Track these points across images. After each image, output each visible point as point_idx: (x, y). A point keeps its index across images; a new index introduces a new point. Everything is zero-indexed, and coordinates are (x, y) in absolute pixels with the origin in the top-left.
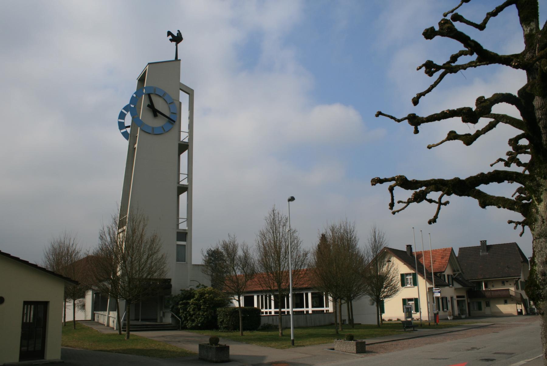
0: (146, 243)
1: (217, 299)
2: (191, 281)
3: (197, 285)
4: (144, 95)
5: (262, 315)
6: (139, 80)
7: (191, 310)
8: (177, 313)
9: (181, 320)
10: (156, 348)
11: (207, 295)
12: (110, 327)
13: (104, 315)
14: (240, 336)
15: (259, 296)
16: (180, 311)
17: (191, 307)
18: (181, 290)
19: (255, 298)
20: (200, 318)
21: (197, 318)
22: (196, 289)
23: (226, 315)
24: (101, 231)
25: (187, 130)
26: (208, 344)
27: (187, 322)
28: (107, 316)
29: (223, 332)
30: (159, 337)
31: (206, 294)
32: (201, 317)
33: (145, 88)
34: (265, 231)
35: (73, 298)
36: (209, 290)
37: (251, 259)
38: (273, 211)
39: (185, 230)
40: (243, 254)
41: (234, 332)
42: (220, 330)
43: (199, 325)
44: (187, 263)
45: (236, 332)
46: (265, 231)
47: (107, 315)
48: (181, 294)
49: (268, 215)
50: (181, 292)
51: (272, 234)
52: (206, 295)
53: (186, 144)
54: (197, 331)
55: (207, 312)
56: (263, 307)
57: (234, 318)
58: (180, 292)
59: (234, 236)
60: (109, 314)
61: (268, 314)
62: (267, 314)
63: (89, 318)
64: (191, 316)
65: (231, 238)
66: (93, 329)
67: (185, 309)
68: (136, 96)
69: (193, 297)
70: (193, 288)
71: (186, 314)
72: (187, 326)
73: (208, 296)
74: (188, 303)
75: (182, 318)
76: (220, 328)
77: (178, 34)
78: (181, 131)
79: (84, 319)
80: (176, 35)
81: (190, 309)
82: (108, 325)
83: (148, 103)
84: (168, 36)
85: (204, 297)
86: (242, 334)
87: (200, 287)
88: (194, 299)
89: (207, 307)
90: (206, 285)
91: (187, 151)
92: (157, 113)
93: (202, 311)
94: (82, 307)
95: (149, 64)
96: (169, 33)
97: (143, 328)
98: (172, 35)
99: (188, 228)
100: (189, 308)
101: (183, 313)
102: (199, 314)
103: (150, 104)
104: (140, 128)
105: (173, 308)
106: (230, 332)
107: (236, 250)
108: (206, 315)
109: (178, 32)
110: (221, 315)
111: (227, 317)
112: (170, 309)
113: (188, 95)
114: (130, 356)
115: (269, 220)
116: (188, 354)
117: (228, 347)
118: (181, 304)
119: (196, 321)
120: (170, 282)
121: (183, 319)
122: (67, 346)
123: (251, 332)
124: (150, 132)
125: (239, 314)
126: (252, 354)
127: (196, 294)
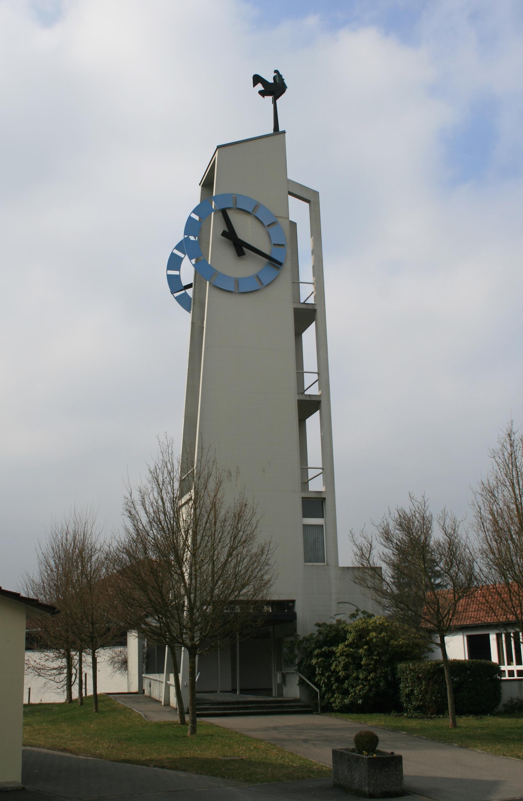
0: (225, 520)
1: (396, 643)
2: (338, 603)
3: (352, 612)
4: (213, 213)
5: (503, 678)
6: (203, 186)
7: (340, 668)
8: (311, 675)
9: (321, 690)
10: (244, 758)
11: (374, 634)
12: (171, 707)
13: (160, 681)
14: (450, 727)
15: (501, 634)
16: (316, 670)
17: (339, 662)
18: (318, 625)
19: (493, 638)
20: (361, 686)
21: (353, 687)
22: (349, 621)
23: (419, 678)
25: (311, 279)
26: (353, 751)
27: (333, 696)
28: (164, 685)
29: (412, 717)
30: (267, 729)
31: (370, 631)
32: (363, 685)
33: (216, 199)
34: (493, 483)
35: (91, 646)
36: (378, 622)
37: (464, 550)
38: (509, 435)
39: (320, 492)
40: (445, 537)
41: (439, 717)
42: (405, 715)
43: (360, 702)
44: (327, 565)
45: (443, 717)
46: (493, 483)
47: (164, 681)
48: (317, 633)
49: (499, 446)
50: (317, 628)
51: (510, 488)
52: (371, 634)
53: (310, 307)
54: (355, 716)
55: (376, 672)
56: (512, 661)
57: (437, 687)
58: (315, 630)
59: (423, 497)
61: (516, 677)
62: (514, 676)
63: (135, 688)
65: (416, 503)
66: (132, 710)
67: (326, 667)
68: (200, 218)
69: (345, 639)
70: (343, 619)
71: (329, 678)
72: (333, 705)
73: (376, 637)
74: (333, 653)
75: (322, 687)
76: (406, 710)
77: (274, 78)
78: (301, 281)
79: (126, 691)
80: (271, 81)
81: (336, 666)
83: (223, 227)
84: (255, 84)
85: (368, 638)
86: (455, 725)
87: (358, 617)
88: (346, 643)
89: (376, 660)
90: (371, 612)
91: (313, 325)
92: (244, 249)
93: (364, 670)
95: (219, 147)
96: (257, 79)
97: (239, 708)
99: (326, 489)
100: (334, 664)
101: (322, 674)
102: (357, 678)
103: (227, 230)
104: (209, 284)
105: (301, 663)
106: (427, 718)
107: (429, 529)
108: (373, 679)
109: (276, 74)
110: (407, 679)
111: (421, 684)
112: (296, 668)
113: (307, 205)
114: (182, 774)
115: (501, 456)
116: (313, 772)
117: (400, 758)
118: (317, 656)
119: (353, 694)
120: (293, 607)
121: (324, 689)
122: (64, 750)
123: (476, 719)
124: (231, 288)
125: (444, 678)
126: (470, 775)
127: (351, 632)
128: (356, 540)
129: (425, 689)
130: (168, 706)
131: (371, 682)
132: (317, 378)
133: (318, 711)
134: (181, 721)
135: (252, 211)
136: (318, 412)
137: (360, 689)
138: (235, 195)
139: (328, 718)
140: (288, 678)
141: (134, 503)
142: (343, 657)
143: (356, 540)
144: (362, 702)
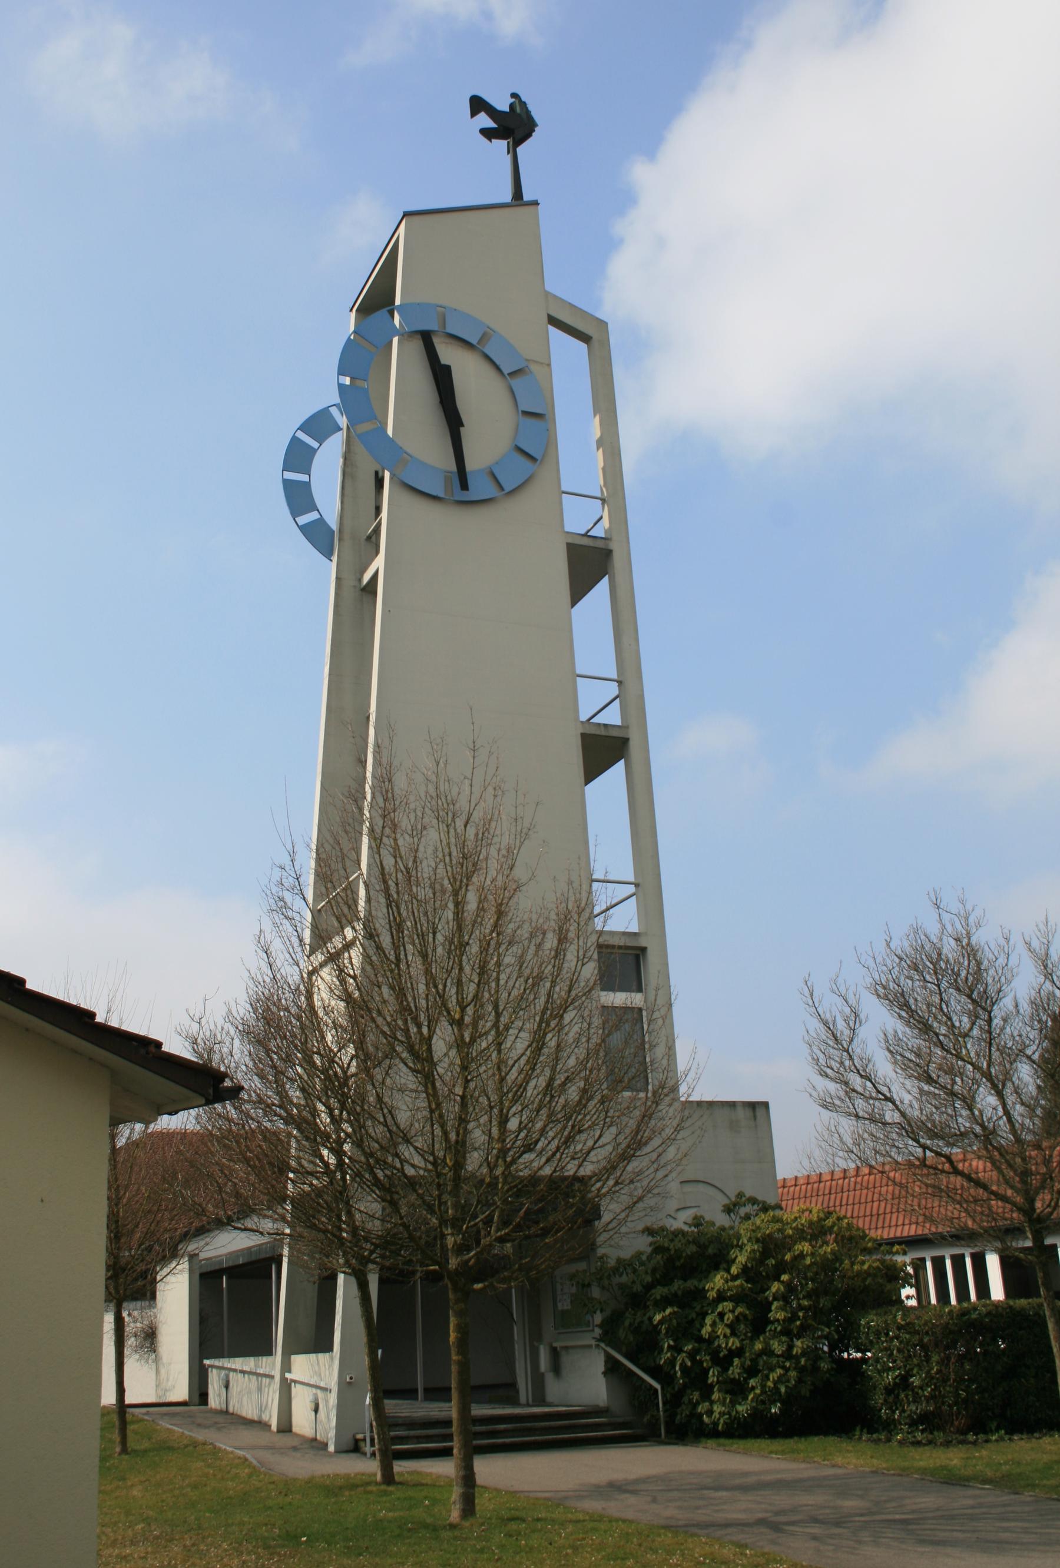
4: (395, 340)
11: (805, 1247)
12: (297, 1435)
24: (277, 874)
30: (616, 1488)
32: (783, 1367)
53: (600, 544)
58: (643, 1244)
59: (962, 902)
60: (286, 1367)
63: (180, 1390)
64: (723, 1362)
68: (352, 379)
71: (692, 1355)
76: (889, 1426)
77: (512, 106)
79: (152, 1399)
82: (286, 1427)
84: (474, 113)
90: (771, 1201)
94: (145, 1339)
95: (406, 214)
96: (478, 105)
98: (492, 112)
104: (391, 479)
108: (804, 1353)
109: (513, 100)
111: (928, 1359)
112: (598, 1331)
113: (583, 346)
119: (758, 1391)
128: (820, 1002)
129: (939, 1372)
130: (288, 1434)
131: (803, 1361)
132: (616, 693)
133: (660, 1436)
134: (383, 1475)
135: (479, 343)
136: (621, 765)
137: (778, 1377)
138: (441, 307)
139: (746, 1452)
140: (566, 1359)
141: (301, 880)
142: (725, 1303)
143: (820, 1002)
144: (780, 1409)
